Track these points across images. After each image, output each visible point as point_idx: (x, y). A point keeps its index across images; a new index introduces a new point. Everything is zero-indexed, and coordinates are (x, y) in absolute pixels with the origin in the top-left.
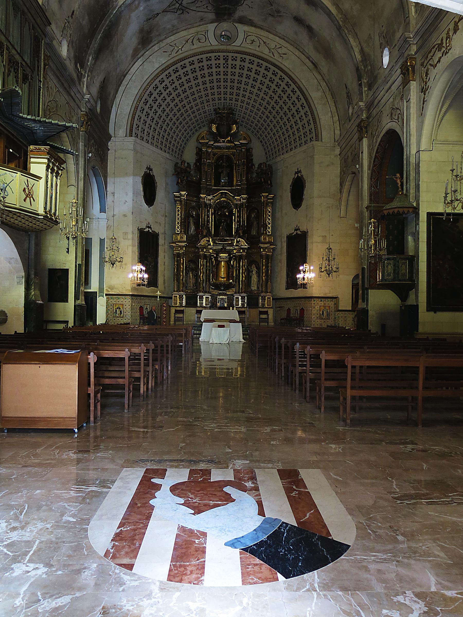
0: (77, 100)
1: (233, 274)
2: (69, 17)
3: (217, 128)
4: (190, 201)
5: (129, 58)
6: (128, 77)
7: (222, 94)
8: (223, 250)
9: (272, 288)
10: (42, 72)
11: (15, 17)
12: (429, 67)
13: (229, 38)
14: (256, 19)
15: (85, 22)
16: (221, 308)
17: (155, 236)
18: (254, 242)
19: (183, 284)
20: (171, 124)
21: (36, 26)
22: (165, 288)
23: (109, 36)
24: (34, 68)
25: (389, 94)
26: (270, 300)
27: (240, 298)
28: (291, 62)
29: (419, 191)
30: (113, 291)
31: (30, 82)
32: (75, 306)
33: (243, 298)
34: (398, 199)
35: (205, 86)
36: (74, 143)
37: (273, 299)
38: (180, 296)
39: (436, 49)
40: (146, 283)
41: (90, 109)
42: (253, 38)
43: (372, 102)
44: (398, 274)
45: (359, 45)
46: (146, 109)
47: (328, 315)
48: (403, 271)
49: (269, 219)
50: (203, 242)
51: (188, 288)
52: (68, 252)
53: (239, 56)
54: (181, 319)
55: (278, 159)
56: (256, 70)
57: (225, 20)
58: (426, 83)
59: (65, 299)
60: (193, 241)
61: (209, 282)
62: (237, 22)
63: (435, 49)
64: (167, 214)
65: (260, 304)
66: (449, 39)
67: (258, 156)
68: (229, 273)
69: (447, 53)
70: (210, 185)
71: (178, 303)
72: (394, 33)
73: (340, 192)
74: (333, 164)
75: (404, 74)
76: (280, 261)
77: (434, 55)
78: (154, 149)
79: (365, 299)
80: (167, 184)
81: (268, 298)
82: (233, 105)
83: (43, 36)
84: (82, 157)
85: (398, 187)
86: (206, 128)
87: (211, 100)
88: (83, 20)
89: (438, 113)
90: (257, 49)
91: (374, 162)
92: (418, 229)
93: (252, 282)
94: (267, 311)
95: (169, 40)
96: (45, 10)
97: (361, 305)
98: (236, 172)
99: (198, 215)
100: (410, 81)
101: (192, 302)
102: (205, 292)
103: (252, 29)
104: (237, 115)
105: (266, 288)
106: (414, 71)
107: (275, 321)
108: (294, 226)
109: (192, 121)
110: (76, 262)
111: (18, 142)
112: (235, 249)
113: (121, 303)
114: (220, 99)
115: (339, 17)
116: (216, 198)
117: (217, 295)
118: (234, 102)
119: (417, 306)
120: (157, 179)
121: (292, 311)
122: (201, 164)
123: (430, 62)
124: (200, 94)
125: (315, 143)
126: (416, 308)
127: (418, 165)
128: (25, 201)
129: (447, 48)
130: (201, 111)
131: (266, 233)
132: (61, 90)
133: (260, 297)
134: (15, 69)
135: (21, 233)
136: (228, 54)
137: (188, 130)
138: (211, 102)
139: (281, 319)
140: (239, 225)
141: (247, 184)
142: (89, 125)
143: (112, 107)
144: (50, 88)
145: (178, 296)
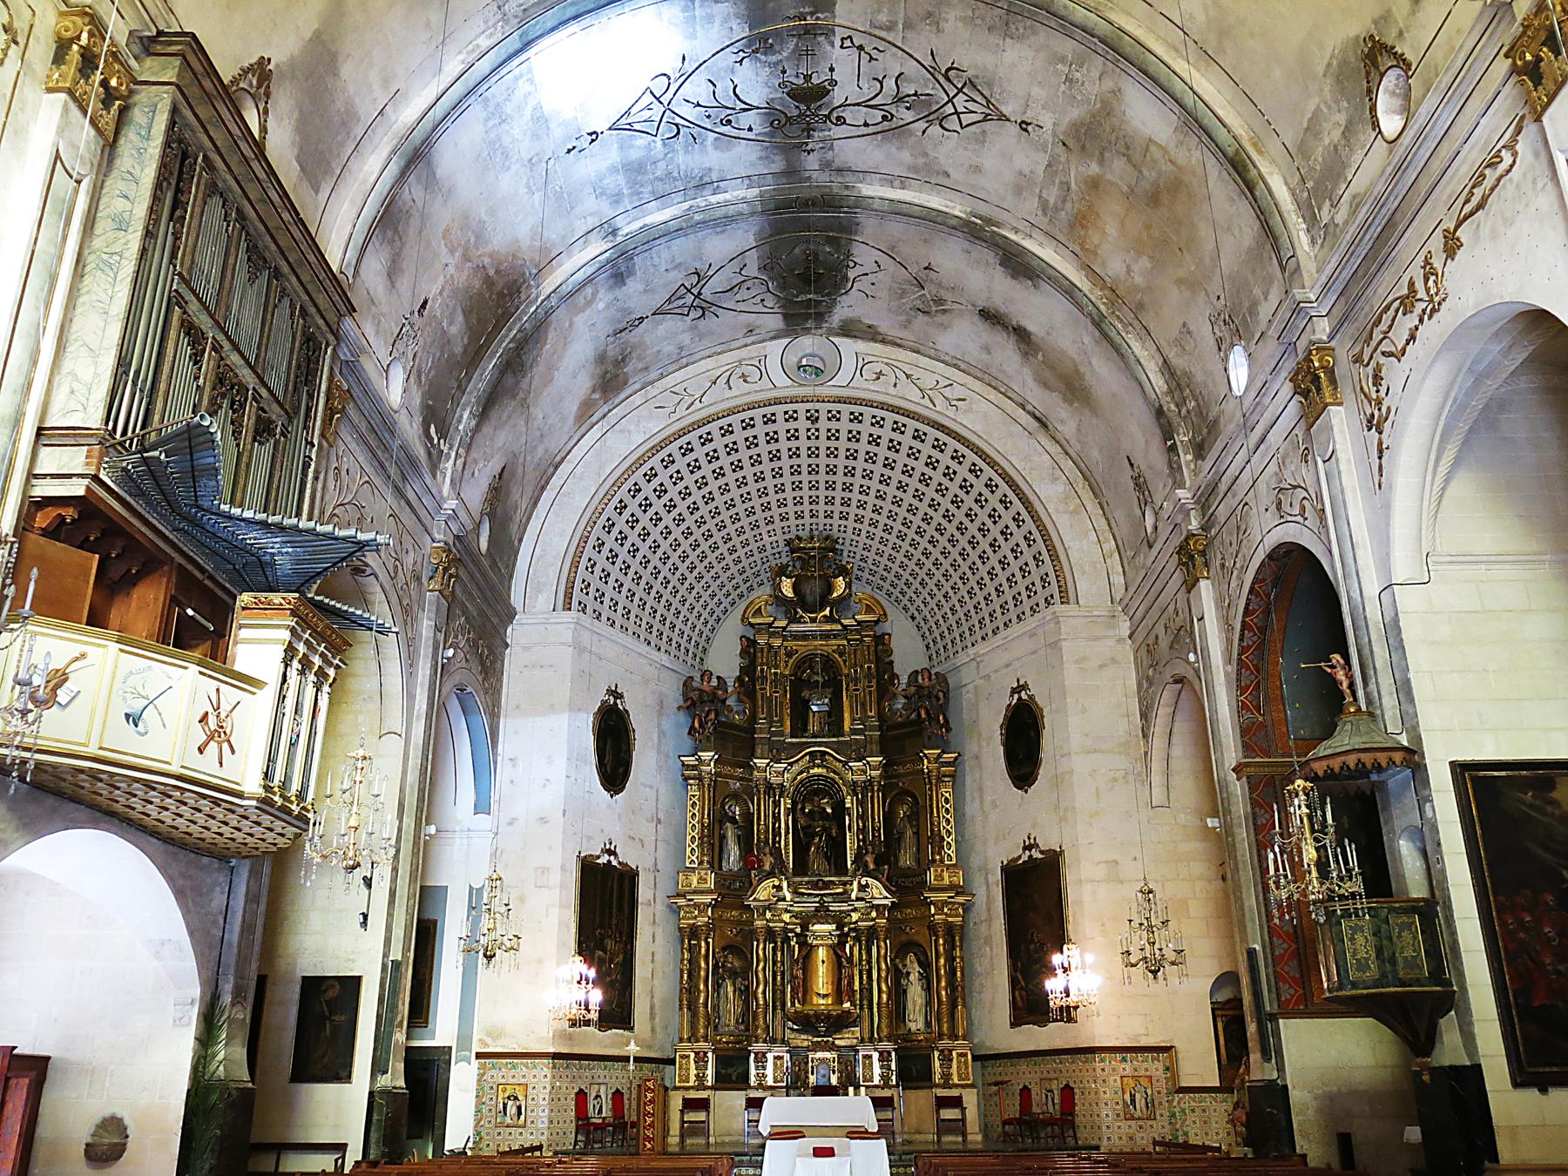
0: (422, 513)
1: (851, 983)
2: (412, 313)
3: (795, 587)
4: (726, 776)
5: (571, 420)
6: (565, 468)
7: (806, 503)
8: (822, 914)
9: (970, 1023)
10: (318, 423)
11: (252, 279)
12: (1382, 360)
13: (818, 372)
14: (885, 326)
15: (456, 328)
16: (821, 1091)
17: (627, 879)
18: (908, 887)
19: (707, 1015)
20: (674, 582)
21: (313, 310)
22: (653, 1030)
23: (515, 365)
24: (295, 407)
25: (1262, 458)
26: (966, 1062)
27: (876, 1055)
28: (982, 417)
29: (1412, 700)
30: (499, 1042)
31: (277, 443)
32: (371, 1094)
33: (885, 1057)
34: (1348, 727)
35: (761, 485)
36: (408, 614)
37: (975, 1058)
38: (697, 1054)
39: (1397, 311)
40: (594, 1016)
41: (457, 537)
42: (878, 367)
43: (1215, 487)
44: (1393, 961)
45: (1157, 355)
46: (610, 542)
47: (1150, 1104)
48: (1409, 953)
49: (948, 822)
50: (764, 891)
51: (721, 1030)
52: (364, 924)
53: (846, 409)
54: (699, 1129)
55: (962, 658)
56: (891, 441)
57: (807, 331)
58: (1379, 403)
59: (341, 1073)
60: (733, 891)
61: (783, 1009)
62: (838, 335)
63: (1391, 312)
64: (661, 816)
65: (938, 1076)
66: (1433, 278)
67: (907, 655)
68: (840, 980)
69: (1434, 311)
70: (781, 734)
71: (692, 1078)
72: (1253, 310)
73: (1145, 736)
74: (1114, 661)
75: (1305, 394)
76: (988, 941)
77: (1390, 327)
78: (628, 640)
79: (1271, 1049)
80: (662, 734)
81: (960, 1055)
82: (835, 528)
83: (331, 338)
84: (426, 656)
85: (1342, 692)
86: (767, 590)
87: (777, 519)
88: (451, 323)
89: (1429, 478)
90: (892, 390)
91: (1241, 640)
92: (1429, 814)
93: (910, 1006)
94: (960, 1097)
95: (668, 382)
96: (345, 286)
97: (1259, 1070)
98: (850, 697)
99: (748, 816)
100: (1326, 405)
101: (732, 1073)
102: (774, 1041)
103: (877, 348)
104: (845, 554)
105: (953, 1026)
106: (1333, 381)
107: (985, 1129)
108: (1020, 839)
109: (729, 573)
110: (385, 955)
111: (220, 593)
112: (855, 910)
113: (523, 1081)
114: (799, 516)
115: (1096, 295)
116: (796, 768)
117: (808, 1049)
118: (836, 521)
119: (1477, 1069)
120: (637, 720)
121: (1037, 1095)
122: (753, 681)
123: (1382, 348)
124: (748, 505)
125: (1058, 608)
126: (1473, 1074)
127: (1393, 628)
128: (201, 751)
129: (1431, 301)
130: (753, 546)
131: (942, 861)
132: (377, 481)
133: (936, 1054)
134: (233, 403)
135: (205, 860)
136: (818, 406)
137: (720, 595)
138: (778, 524)
139: (1005, 1123)
140: (864, 840)
141: (880, 728)
142: (451, 576)
143: (521, 540)
144: (344, 473)
145: (692, 1055)
